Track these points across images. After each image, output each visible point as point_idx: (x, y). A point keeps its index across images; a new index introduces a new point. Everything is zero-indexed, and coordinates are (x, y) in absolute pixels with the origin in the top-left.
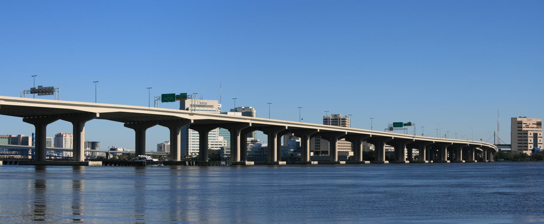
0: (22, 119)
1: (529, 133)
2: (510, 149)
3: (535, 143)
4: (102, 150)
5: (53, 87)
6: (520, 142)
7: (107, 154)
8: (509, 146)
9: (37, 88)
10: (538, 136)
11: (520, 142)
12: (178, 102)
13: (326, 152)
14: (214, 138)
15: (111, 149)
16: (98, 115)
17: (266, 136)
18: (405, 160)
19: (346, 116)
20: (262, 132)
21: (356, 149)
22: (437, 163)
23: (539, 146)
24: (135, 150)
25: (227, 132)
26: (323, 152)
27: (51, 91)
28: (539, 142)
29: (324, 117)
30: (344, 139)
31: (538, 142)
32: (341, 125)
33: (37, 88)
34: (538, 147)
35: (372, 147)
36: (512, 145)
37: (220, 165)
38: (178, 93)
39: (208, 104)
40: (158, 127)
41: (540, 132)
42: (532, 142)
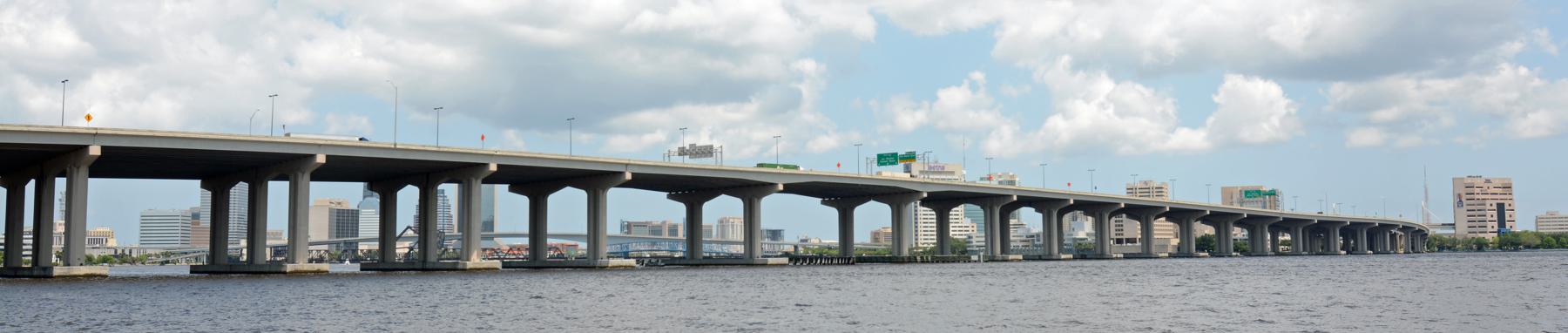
0: (665, 194)
1: (1488, 202)
2: (1453, 231)
3: (1502, 221)
4: (789, 242)
5: (712, 146)
6: (1471, 224)
7: (796, 247)
8: (1453, 225)
9: (688, 148)
10: (1507, 207)
11: (1471, 224)
12: (901, 165)
13: (1133, 241)
14: (925, 221)
15: (802, 241)
16: (781, 187)
17: (1040, 216)
18: (1339, 249)
19: (1163, 183)
20: (1033, 210)
21: (1185, 232)
22: (1298, 257)
23: (1508, 225)
24: (838, 242)
25: (977, 210)
26: (1128, 241)
27: (710, 152)
28: (1507, 218)
29: (1128, 184)
30: (1163, 219)
31: (1496, 223)
32: (1139, 194)
33: (688, 148)
34: (1508, 227)
35: (1209, 230)
36: (1457, 225)
37: (969, 262)
38: (901, 152)
39: (946, 170)
40: (568, 191)
41: (1510, 202)
42: (1495, 218)
